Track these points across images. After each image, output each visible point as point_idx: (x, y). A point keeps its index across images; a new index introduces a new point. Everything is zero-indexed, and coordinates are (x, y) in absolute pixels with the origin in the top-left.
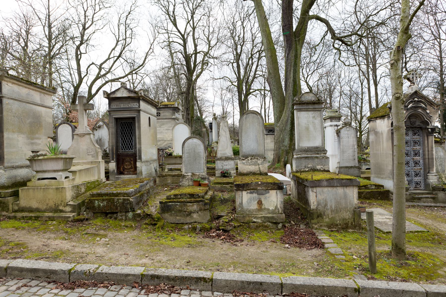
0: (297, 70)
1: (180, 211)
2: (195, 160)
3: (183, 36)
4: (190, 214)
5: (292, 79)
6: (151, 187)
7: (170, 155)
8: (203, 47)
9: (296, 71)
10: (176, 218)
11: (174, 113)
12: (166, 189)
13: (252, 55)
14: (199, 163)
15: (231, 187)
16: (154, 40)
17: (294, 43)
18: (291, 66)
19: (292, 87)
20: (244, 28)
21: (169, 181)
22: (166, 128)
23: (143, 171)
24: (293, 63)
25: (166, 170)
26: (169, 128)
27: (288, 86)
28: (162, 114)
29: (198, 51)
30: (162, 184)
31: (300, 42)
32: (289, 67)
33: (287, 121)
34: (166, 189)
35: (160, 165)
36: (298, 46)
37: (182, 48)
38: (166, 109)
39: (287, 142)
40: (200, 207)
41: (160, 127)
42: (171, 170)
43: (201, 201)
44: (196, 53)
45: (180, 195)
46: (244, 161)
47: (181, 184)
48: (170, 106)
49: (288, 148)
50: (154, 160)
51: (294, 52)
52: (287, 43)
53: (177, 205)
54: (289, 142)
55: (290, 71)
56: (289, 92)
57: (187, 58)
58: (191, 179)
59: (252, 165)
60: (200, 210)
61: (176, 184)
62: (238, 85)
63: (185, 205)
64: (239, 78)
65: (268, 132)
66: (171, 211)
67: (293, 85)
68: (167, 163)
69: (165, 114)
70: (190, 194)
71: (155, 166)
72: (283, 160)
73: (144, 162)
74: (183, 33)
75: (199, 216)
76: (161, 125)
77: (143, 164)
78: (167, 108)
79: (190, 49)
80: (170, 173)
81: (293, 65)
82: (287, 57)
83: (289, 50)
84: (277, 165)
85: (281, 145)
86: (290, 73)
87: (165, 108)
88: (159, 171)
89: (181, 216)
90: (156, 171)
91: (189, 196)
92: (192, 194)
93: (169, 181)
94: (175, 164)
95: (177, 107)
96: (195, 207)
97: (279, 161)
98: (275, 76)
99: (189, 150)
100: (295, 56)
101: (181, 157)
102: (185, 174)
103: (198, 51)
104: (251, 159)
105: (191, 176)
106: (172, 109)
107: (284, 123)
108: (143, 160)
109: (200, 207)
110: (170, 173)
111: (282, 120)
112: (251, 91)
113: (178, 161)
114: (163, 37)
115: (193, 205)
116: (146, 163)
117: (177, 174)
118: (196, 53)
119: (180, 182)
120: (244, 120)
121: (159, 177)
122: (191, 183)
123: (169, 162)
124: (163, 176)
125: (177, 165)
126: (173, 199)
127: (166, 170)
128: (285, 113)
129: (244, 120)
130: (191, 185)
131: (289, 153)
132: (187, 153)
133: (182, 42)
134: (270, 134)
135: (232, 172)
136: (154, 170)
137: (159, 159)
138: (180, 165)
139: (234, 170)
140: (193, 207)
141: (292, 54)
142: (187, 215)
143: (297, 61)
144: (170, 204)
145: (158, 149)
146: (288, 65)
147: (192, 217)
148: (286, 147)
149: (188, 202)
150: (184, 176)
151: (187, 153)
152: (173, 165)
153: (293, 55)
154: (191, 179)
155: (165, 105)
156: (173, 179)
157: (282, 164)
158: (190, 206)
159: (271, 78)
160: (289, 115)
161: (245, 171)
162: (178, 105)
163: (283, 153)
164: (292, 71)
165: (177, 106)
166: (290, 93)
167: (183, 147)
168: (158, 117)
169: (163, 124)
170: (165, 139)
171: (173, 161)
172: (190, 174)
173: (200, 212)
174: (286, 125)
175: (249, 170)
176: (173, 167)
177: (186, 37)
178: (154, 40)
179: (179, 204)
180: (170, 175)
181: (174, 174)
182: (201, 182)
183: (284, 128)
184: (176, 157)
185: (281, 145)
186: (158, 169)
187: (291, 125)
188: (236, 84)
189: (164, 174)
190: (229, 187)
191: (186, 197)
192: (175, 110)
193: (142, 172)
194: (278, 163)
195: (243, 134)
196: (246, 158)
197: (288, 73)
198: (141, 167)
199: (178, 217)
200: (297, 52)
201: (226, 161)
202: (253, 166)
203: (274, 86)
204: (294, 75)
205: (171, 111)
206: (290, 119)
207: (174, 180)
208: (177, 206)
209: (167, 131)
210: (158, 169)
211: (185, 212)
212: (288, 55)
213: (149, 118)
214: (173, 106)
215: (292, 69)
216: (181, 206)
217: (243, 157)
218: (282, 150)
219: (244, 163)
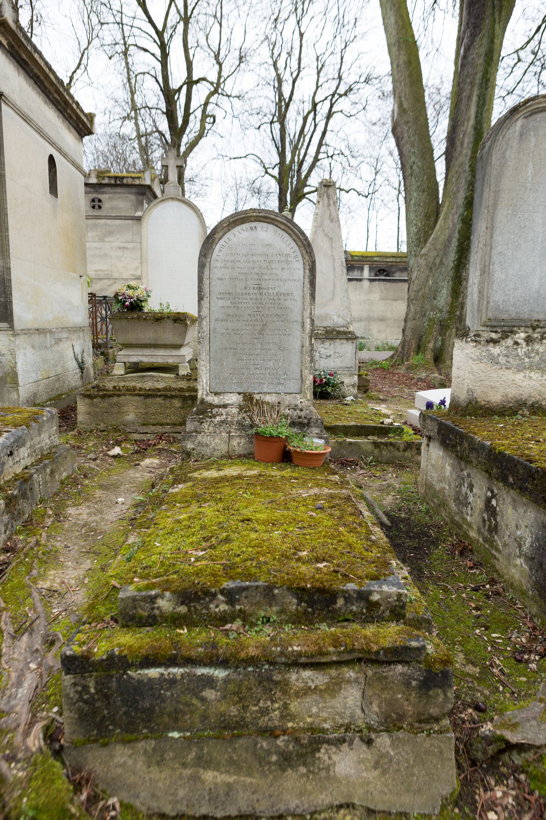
0: (488, 98)
1: (231, 729)
2: (262, 332)
3: (160, 34)
4: (307, 747)
5: (472, 122)
6: (48, 458)
7: (136, 306)
8: (204, 67)
9: (484, 100)
10: (195, 778)
11: (142, 203)
12: (117, 450)
13: (315, 105)
14: (282, 349)
15: (376, 445)
16: (89, 43)
17: (489, 12)
18: (472, 84)
19: (471, 146)
20: (301, 35)
21: (131, 417)
22: (118, 244)
23: (20, 369)
24: (479, 76)
25: (119, 370)
26: (126, 245)
27: (458, 144)
28: (107, 205)
29: (195, 78)
30: (102, 426)
31: (503, 13)
32: (467, 87)
33: (449, 241)
34: (117, 450)
35: (96, 346)
36: (497, 26)
37: (159, 66)
38: (119, 190)
39: (444, 298)
40: (391, 703)
41: (102, 240)
42: (136, 368)
43: (399, 655)
44: (190, 83)
45: (231, 596)
46: (495, 350)
47: (189, 446)
48: (130, 181)
49: (445, 315)
50: (79, 329)
51: (485, 41)
52: (469, 14)
53: (210, 682)
54: (449, 300)
55: (469, 98)
56: (461, 159)
57: (169, 95)
58: (241, 425)
59: (530, 368)
60: (391, 723)
61: (160, 429)
62: (280, 174)
63: (267, 684)
64: (282, 162)
65: (376, 275)
66: (158, 733)
67: (472, 139)
68: (122, 339)
69: (114, 203)
70: (301, 593)
71: (78, 350)
72: (431, 345)
73: (27, 332)
74: (160, 28)
75: (381, 763)
76: (105, 236)
77: (21, 341)
78: (122, 185)
79: (177, 77)
80: (136, 381)
81: (478, 81)
82: (465, 57)
83: (473, 36)
84: (415, 359)
85: (428, 307)
86: (468, 106)
87: (115, 185)
88: (94, 365)
89: (234, 765)
90: (81, 367)
91: (292, 604)
92: (321, 591)
93: (131, 412)
94: (156, 346)
95: (149, 187)
96: (350, 700)
97: (419, 349)
98: (416, 119)
99: (234, 279)
100: (486, 55)
101: (180, 319)
102: (210, 399)
103: (195, 78)
104: (529, 340)
105: (241, 408)
106: (134, 190)
107: (438, 246)
108: (18, 325)
109: (391, 703)
110: (136, 381)
111: (436, 239)
112: (306, 190)
113: (167, 334)
114: (112, 33)
115: (334, 688)
116: (37, 339)
117: (161, 385)
118: (190, 83)
119: (189, 435)
120: (515, 143)
121: (90, 397)
122: (239, 444)
123: (131, 337)
124: (105, 395)
125: (161, 352)
126: (176, 621)
127: (119, 370)
128: (445, 219)
129: (515, 143)
130: (239, 450)
131: (448, 327)
132: (223, 296)
133: (158, 52)
134: (379, 280)
135: (347, 381)
136: (73, 365)
137: (93, 326)
138: (175, 352)
139: (351, 375)
140: (337, 703)
141: (480, 48)
142: (287, 761)
143: (490, 70)
144: (153, 672)
145: (92, 295)
146: (464, 82)
147: (327, 774)
148: (441, 311)
149: (296, 663)
150: (205, 410)
151: (223, 296)
152: (147, 352)
153: (483, 50)
154: (241, 425)
155: (116, 178)
156: (146, 406)
157: (429, 356)
158: (307, 691)
159: (407, 123)
160: (454, 224)
161: (495, 398)
162: (152, 180)
163: (431, 327)
164: (475, 98)
165: (148, 182)
166: (462, 164)
167: (202, 266)
168: (97, 213)
169: (111, 233)
170: (116, 275)
171: (148, 334)
172: (233, 399)
173: (383, 741)
174: (445, 253)
175: (513, 392)
176: (145, 360)
177: (166, 36)
178: (89, 43)
179: (220, 674)
180: (132, 391)
181: (149, 385)
182: (294, 445)
183: (438, 261)
184: (158, 318)
185: (428, 307)
186: (89, 360)
187: (457, 252)
188: (276, 172)
189: (110, 385)
190: (370, 448)
191: (273, 612)
192: (143, 194)
193: (15, 375)
194: (417, 354)
195: (502, 214)
196: (505, 336)
197: (463, 107)
198: (13, 354)
199: (209, 776)
200: (492, 42)
201: (327, 344)
202: (535, 375)
203: (413, 146)
204: (477, 112)
205: (132, 197)
206: (457, 235)
207: (152, 410)
208: (210, 694)
209: (120, 253)
210: (89, 360)
211: (271, 733)
212: (467, 50)
213: (51, 159)
214: (137, 182)
215: (476, 92)
216: (236, 693)
217: (493, 328)
218: (430, 320)
219: (494, 360)
